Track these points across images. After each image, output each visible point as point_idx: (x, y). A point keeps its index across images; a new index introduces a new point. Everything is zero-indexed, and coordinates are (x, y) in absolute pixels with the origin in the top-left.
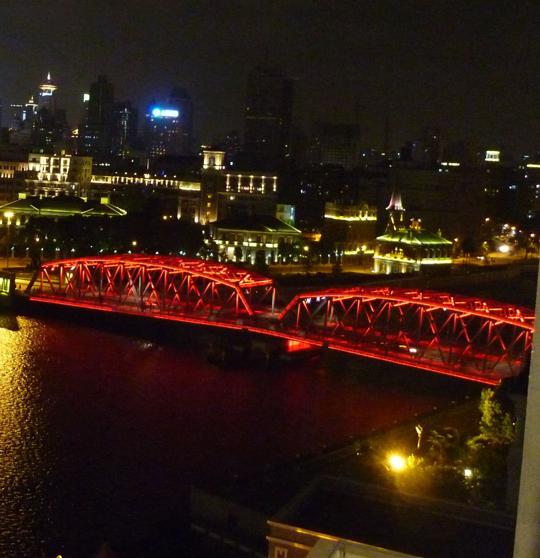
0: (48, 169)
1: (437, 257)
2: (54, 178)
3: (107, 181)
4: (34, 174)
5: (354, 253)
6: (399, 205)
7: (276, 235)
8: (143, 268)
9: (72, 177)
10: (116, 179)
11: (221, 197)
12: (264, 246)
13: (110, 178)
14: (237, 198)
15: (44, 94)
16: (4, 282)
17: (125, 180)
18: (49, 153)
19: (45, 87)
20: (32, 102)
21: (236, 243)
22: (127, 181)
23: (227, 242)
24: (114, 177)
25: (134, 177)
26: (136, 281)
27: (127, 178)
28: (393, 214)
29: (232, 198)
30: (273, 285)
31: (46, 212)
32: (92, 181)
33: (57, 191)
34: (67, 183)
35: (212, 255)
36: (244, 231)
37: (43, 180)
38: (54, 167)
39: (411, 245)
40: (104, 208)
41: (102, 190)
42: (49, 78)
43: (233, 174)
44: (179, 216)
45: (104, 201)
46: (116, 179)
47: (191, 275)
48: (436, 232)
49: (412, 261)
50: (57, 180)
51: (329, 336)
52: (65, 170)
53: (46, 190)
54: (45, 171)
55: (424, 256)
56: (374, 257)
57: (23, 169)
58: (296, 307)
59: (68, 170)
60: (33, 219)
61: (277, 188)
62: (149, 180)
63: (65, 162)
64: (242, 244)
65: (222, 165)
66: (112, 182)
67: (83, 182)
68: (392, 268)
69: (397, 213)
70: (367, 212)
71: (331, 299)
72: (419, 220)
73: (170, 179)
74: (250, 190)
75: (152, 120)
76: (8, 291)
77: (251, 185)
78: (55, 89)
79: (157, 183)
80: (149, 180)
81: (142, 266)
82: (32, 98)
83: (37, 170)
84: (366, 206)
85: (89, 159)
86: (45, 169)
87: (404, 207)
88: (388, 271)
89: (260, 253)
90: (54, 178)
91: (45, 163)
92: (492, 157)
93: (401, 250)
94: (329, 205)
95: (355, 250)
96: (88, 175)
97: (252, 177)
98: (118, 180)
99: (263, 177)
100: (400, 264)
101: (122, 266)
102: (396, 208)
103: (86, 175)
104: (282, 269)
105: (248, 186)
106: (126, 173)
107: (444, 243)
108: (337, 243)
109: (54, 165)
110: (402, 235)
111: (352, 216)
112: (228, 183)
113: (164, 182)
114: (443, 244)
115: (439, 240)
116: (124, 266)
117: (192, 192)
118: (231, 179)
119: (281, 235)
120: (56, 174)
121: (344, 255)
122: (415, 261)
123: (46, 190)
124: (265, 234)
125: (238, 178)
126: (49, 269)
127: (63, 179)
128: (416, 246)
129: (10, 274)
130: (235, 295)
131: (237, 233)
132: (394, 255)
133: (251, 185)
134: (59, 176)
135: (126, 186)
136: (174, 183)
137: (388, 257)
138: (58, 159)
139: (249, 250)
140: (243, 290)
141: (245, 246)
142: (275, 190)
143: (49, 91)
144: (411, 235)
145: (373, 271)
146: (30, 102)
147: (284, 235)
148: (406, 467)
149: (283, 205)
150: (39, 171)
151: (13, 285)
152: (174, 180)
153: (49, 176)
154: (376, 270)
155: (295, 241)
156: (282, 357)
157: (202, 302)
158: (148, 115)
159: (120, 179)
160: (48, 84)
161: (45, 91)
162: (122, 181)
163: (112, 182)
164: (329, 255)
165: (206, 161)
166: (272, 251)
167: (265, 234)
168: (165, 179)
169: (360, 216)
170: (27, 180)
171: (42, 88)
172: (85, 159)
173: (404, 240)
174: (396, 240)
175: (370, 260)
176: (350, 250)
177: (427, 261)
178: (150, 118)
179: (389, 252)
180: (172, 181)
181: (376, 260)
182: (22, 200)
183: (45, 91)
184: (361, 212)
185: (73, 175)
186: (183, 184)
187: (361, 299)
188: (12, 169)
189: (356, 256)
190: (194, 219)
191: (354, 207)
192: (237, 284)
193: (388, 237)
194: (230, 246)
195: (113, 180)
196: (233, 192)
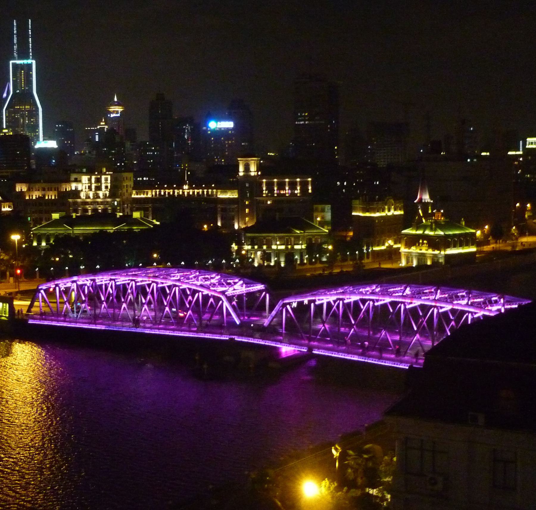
0: (90, 188)
2: (97, 196)
3: (147, 195)
4: (76, 193)
6: (426, 198)
7: (304, 237)
8: (134, 283)
9: (113, 193)
10: (156, 192)
11: (259, 202)
12: (293, 248)
13: (150, 192)
14: (274, 202)
15: (112, 116)
16: (3, 306)
17: (165, 193)
18: (90, 172)
19: (112, 109)
20: (104, 123)
21: (265, 247)
22: (167, 193)
23: (256, 247)
24: (154, 191)
25: (174, 189)
26: (157, 292)
27: (167, 191)
28: (421, 207)
29: (269, 202)
30: (266, 290)
31: (79, 230)
32: (133, 196)
33: (100, 208)
34: (109, 200)
35: (237, 261)
36: (272, 235)
37: (86, 198)
38: (96, 185)
39: (435, 236)
40: (136, 222)
41: (139, 204)
42: (116, 100)
43: (292, 178)
44: (219, 224)
45: (136, 215)
46: (156, 192)
47: (179, 286)
48: (459, 221)
49: (437, 252)
50: (99, 197)
51: (314, 340)
52: (106, 187)
53: (90, 208)
54: (87, 190)
55: (447, 246)
56: (400, 251)
57: (66, 189)
58: (282, 311)
59: (109, 187)
60: (57, 238)
61: (312, 189)
62: (188, 191)
63: (106, 180)
64: (271, 248)
65: (258, 171)
66: (152, 195)
67: (124, 197)
68: (419, 260)
69: (425, 206)
70: (393, 207)
71: (314, 301)
72: (442, 211)
73: (160, 189)
74: (286, 193)
75: (209, 132)
76: (7, 316)
77: (287, 188)
78: (122, 110)
79: (196, 194)
80: (188, 191)
81: (132, 280)
82: (103, 120)
83: (80, 189)
85: (131, 175)
86: (87, 187)
87: (431, 199)
88: (415, 264)
89: (289, 255)
90: (97, 196)
91: (87, 182)
92: (532, 143)
93: (425, 242)
94: (356, 203)
95: (383, 245)
96: (130, 190)
97: (287, 180)
98: (158, 193)
99: (298, 180)
100: (425, 256)
101: (113, 282)
102: (423, 201)
103: (127, 191)
104: (308, 270)
106: (175, 186)
107: (467, 231)
108: (365, 240)
109: (95, 183)
110: (425, 227)
111: (378, 211)
112: (264, 189)
114: (466, 233)
115: (461, 228)
116: (115, 283)
117: (229, 199)
118: (267, 184)
119: (309, 235)
120: (98, 192)
121: (372, 250)
122: (439, 252)
123: (89, 208)
124: (292, 236)
125: (274, 182)
127: (105, 196)
128: (439, 237)
129: (8, 299)
130: (222, 304)
132: (419, 248)
133: (287, 188)
134: (101, 194)
135: (206, 198)
136: (212, 192)
138: (99, 177)
139: (278, 253)
140: (230, 299)
141: (274, 250)
142: (310, 191)
143: (117, 112)
144: (434, 227)
145: (401, 265)
146: (102, 123)
147: (312, 235)
148: (319, 494)
149: (323, 206)
150: (82, 190)
151: (12, 307)
152: (212, 188)
153: (91, 194)
154: (403, 263)
155: (323, 241)
156: (272, 365)
157: (191, 313)
158: (204, 128)
159: (160, 192)
160: (116, 105)
161: (113, 112)
162: (162, 193)
163: (152, 195)
164: (357, 252)
165: (241, 168)
166: (301, 252)
167: (292, 236)
169: (387, 211)
170: (70, 200)
171: (110, 110)
172: (126, 175)
173: (427, 232)
174: (420, 232)
175: (397, 252)
176: (378, 245)
178: (206, 131)
179: (414, 245)
180: (210, 190)
181: (403, 254)
182: (56, 220)
183: (113, 112)
184: (386, 207)
185: (114, 192)
186: (221, 192)
187: (343, 300)
188: (55, 190)
189: (385, 250)
190: (234, 225)
191: (380, 203)
192: (223, 293)
193: (412, 230)
194: (259, 250)
195: (154, 194)
196: (271, 196)
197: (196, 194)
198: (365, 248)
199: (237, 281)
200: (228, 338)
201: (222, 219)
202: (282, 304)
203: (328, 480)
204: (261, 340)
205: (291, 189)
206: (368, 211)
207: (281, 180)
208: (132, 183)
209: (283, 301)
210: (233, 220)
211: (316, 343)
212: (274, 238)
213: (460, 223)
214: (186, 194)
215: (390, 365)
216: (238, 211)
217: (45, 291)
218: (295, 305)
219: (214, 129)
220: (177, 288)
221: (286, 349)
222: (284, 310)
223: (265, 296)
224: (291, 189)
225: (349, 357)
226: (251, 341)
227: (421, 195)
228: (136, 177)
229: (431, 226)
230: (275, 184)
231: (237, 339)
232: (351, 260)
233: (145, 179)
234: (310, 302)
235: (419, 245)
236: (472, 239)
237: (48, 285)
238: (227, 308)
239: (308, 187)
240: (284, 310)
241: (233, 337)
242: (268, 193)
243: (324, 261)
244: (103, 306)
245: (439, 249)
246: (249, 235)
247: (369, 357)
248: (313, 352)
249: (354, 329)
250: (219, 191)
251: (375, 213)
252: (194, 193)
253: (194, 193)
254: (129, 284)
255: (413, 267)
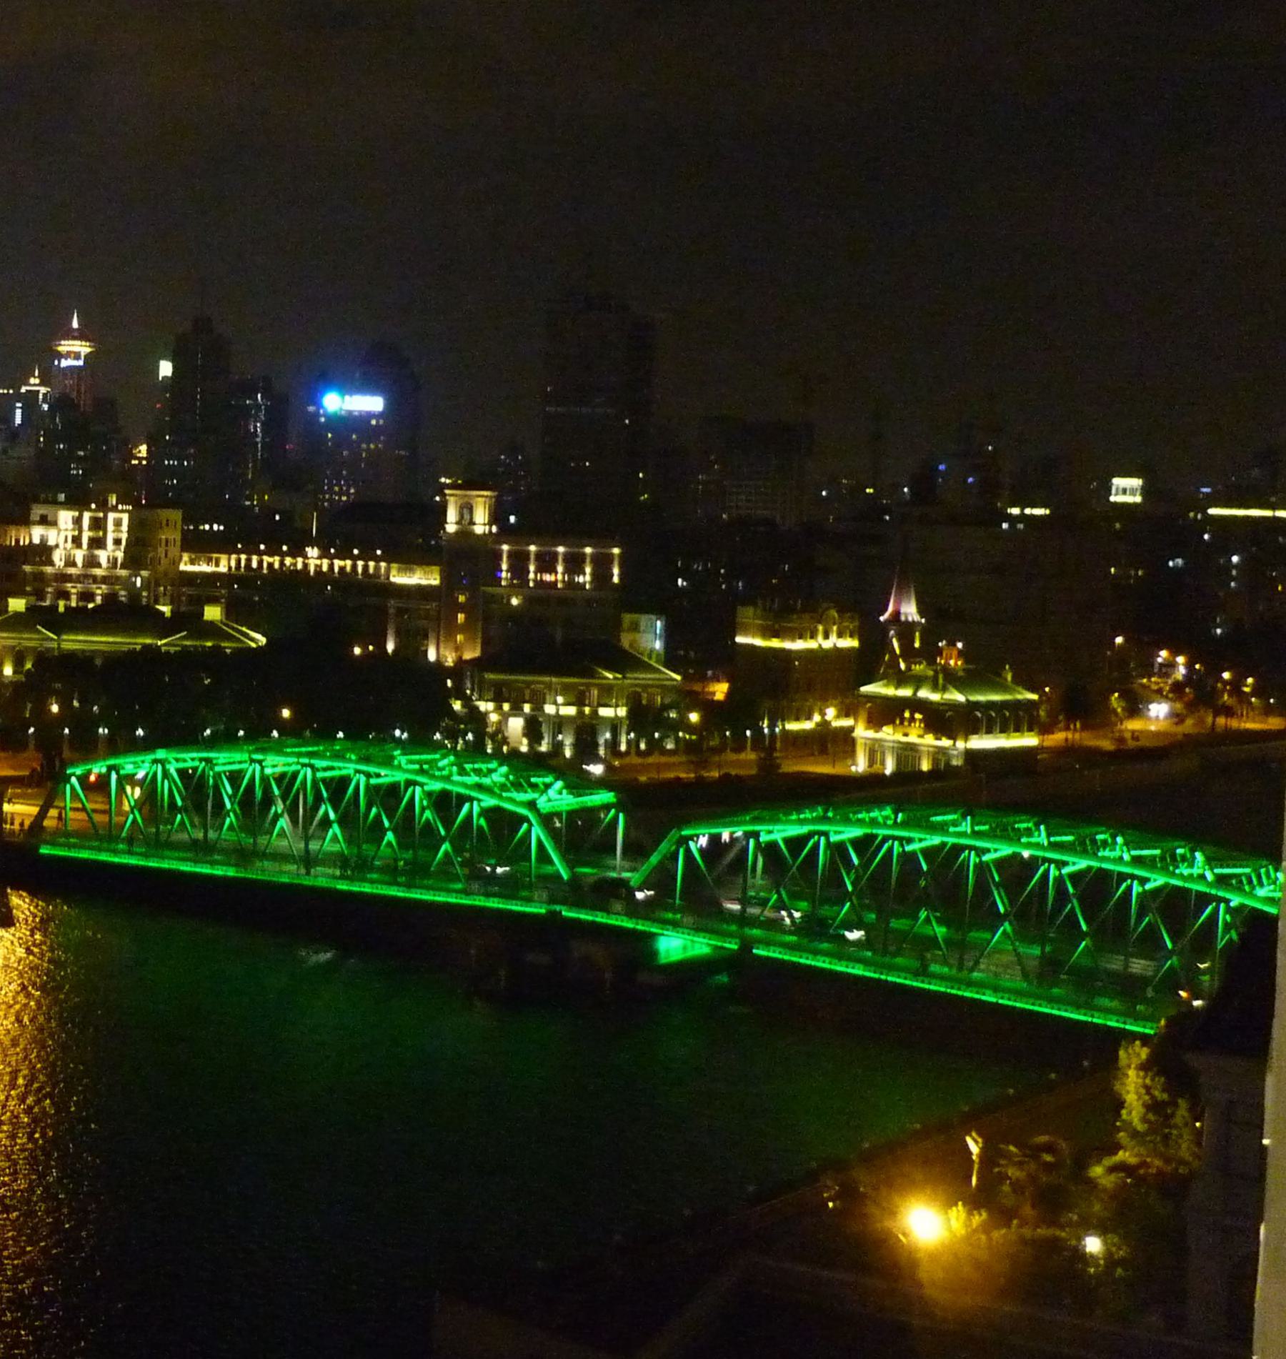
0: (77, 541)
1: (1017, 730)
2: (92, 562)
3: (217, 565)
4: (43, 552)
5: (807, 725)
6: (910, 611)
7: (622, 688)
9: (134, 559)
10: (239, 561)
11: (492, 598)
12: (595, 713)
14: (529, 601)
15: (65, 363)
17: (260, 563)
18: (77, 501)
19: (66, 346)
21: (527, 708)
22: (265, 565)
23: (506, 707)
24: (234, 557)
27: (266, 559)
30: (620, 806)
31: (74, 642)
32: (183, 567)
33: (99, 592)
34: (124, 573)
35: (470, 736)
36: (547, 679)
38: (91, 534)
40: (211, 630)
41: (206, 587)
42: (75, 324)
44: (390, 647)
46: (239, 561)
49: (945, 742)
50: (99, 565)
52: (117, 542)
53: (74, 591)
54: (69, 545)
55: (973, 728)
56: (855, 734)
57: (17, 541)
59: (124, 542)
60: (43, 659)
61: (621, 576)
62: (318, 562)
63: (118, 523)
65: (490, 524)
66: (230, 568)
68: (899, 761)
69: (906, 630)
70: (835, 628)
71: (756, 835)
72: (960, 645)
73: (249, 553)
77: (560, 569)
78: (89, 350)
79: (336, 570)
80: (318, 562)
83: (51, 542)
84: (834, 613)
85: (176, 515)
86: (70, 539)
88: (889, 768)
90: (92, 562)
91: (70, 526)
92: (1124, 491)
93: (918, 716)
94: (747, 614)
95: (809, 718)
97: (561, 549)
100: (917, 751)
102: (903, 618)
105: (553, 570)
107: (1019, 697)
108: (768, 704)
109: (90, 529)
110: (918, 682)
112: (504, 567)
113: (354, 567)
115: (1004, 688)
117: (419, 588)
119: (636, 685)
120: (97, 552)
122: (951, 742)
123: (73, 589)
126: (83, 779)
127: (113, 563)
128: (954, 706)
130: (529, 831)
131: (528, 684)
133: (560, 569)
134: (103, 556)
135: (360, 583)
136: (377, 568)
137: (888, 734)
138: (101, 515)
139: (559, 723)
140: (547, 820)
142: (616, 579)
144: (941, 681)
145: (853, 769)
146: (32, 381)
150: (57, 546)
152: (377, 560)
153: (79, 555)
154: (860, 765)
155: (667, 701)
156: (643, 977)
158: (311, 409)
159: (249, 561)
160: (74, 338)
161: (68, 355)
162: (254, 565)
163: (230, 568)
165: (452, 515)
166: (614, 725)
168: (355, 559)
169: (820, 637)
170: (27, 568)
171: (60, 349)
173: (924, 693)
174: (906, 692)
175: (845, 741)
176: (797, 719)
177: (980, 742)
178: (317, 415)
180: (372, 564)
182: (17, 615)
184: (821, 628)
186: (399, 570)
187: (826, 834)
190: (426, 651)
195: (233, 564)
196: (519, 586)
197: (336, 570)
198: (766, 722)
199: (549, 779)
200: (543, 911)
201: (398, 635)
202: (676, 837)
203: (964, 1205)
204: (625, 918)
205: (570, 570)
206: (776, 634)
207: (603, 551)
208: (177, 536)
209: (680, 829)
210: (426, 637)
211: (756, 932)
212: (549, 686)
213: (1000, 675)
214: (312, 569)
215: (942, 989)
216: (438, 619)
217: (79, 778)
218: (703, 841)
219: (336, 414)
220: (418, 789)
221: (675, 945)
222: (682, 851)
223: (616, 819)
224: (570, 570)
225: (840, 967)
226: (601, 918)
227: (898, 603)
228: (185, 520)
229: (935, 679)
230: (532, 557)
231: (568, 913)
232: (754, 749)
233: (207, 527)
234: (748, 835)
235: (902, 723)
236: (1031, 716)
237: (88, 767)
238: (540, 845)
239: (611, 569)
240: (682, 851)
241: (558, 908)
242: (512, 579)
243: (670, 751)
244: (228, 821)
245: (953, 737)
246: (491, 676)
247: (891, 968)
248: (755, 951)
249: (852, 905)
250: (394, 566)
251: (793, 640)
252: (331, 566)
253: (331, 566)
254: (298, 772)
255: (884, 775)
